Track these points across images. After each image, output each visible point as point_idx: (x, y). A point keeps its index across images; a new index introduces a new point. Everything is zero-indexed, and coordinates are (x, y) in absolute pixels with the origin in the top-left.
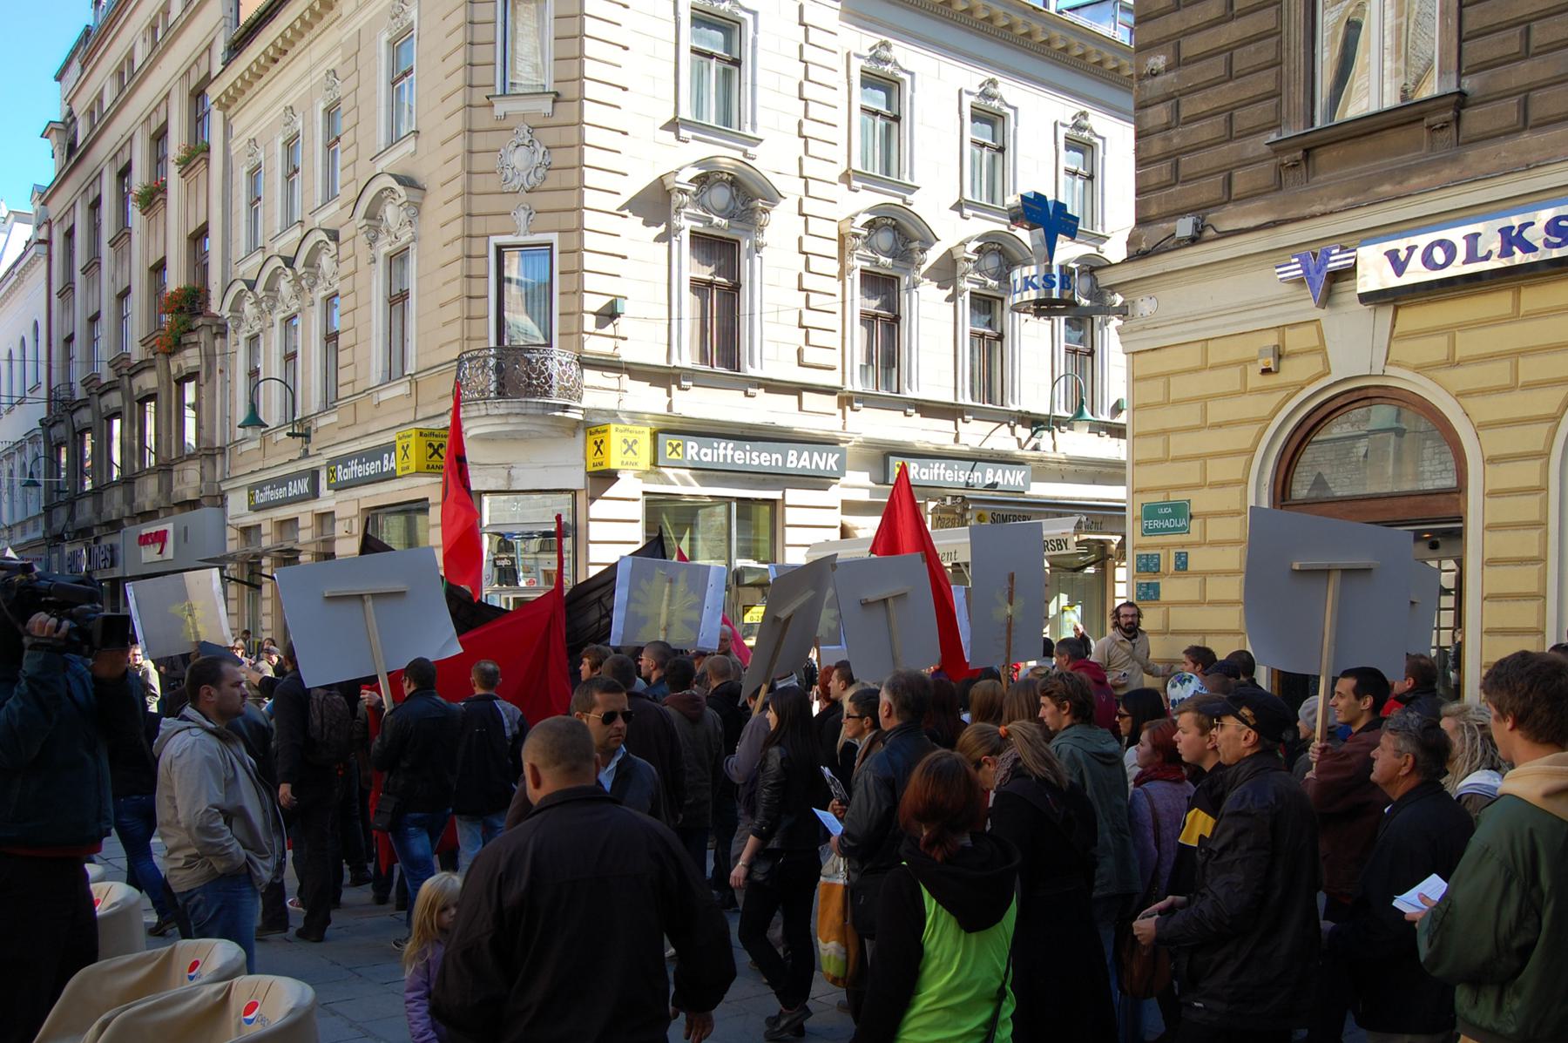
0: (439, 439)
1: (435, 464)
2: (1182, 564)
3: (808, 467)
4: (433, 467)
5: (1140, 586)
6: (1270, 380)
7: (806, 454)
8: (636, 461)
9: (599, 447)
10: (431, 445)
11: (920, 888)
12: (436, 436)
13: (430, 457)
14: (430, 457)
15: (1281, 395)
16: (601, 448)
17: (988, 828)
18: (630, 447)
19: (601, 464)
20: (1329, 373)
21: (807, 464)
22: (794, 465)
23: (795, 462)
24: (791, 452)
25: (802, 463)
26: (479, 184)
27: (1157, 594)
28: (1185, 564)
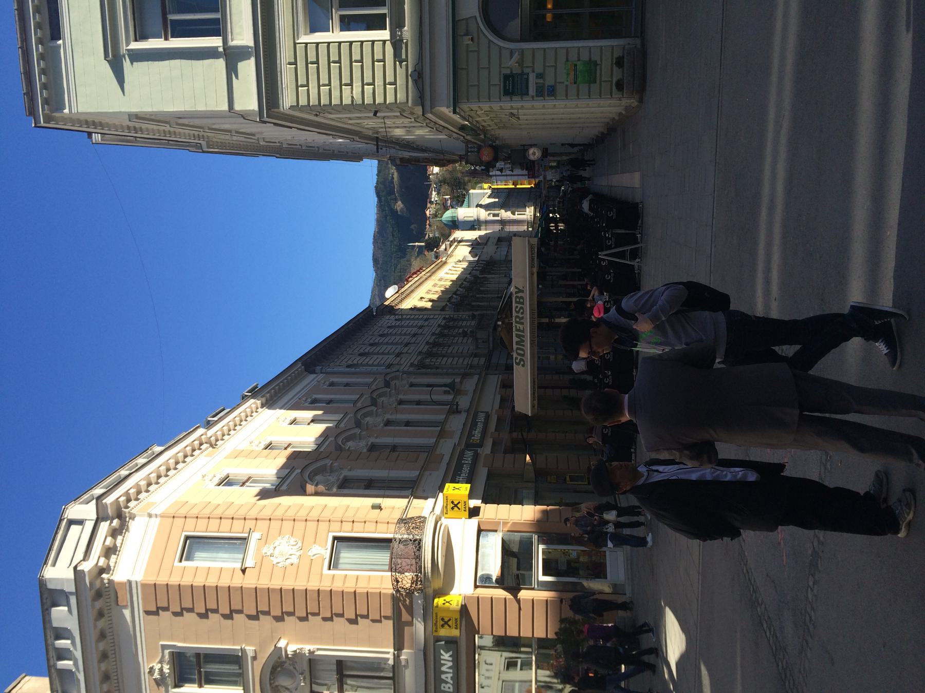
0: (449, 503)
1: (454, 624)
2: (540, 76)
3: (451, 675)
4: (465, 508)
5: (548, 95)
6: (476, 40)
7: (443, 677)
8: (454, 619)
9: (447, 602)
10: (453, 508)
11: (677, 678)
12: (437, 622)
13: (459, 509)
14: (459, 509)
15: (481, 35)
16: (448, 601)
17: (623, 671)
18: (456, 506)
19: (456, 619)
20: (475, 16)
21: (450, 675)
22: (451, 687)
23: (449, 685)
24: (442, 688)
25: (449, 680)
26: (312, 526)
27: (552, 86)
28: (540, 74)
